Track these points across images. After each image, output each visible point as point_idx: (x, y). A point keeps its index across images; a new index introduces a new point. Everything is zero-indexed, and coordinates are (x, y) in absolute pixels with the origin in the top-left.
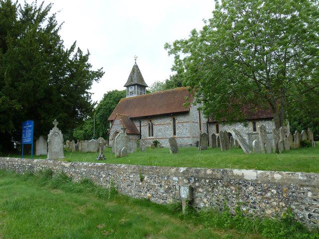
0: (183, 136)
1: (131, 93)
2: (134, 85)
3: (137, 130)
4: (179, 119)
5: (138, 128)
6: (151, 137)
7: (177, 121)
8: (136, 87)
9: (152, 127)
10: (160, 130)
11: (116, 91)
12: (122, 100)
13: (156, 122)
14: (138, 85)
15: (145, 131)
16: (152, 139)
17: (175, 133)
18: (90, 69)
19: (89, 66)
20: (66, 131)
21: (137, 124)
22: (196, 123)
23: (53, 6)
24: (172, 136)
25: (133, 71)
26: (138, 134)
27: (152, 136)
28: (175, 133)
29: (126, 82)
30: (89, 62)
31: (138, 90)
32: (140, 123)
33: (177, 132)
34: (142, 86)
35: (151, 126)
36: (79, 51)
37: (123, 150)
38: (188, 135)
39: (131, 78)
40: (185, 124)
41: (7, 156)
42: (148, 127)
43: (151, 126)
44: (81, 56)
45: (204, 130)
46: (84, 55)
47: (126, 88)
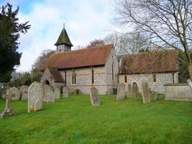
0: (99, 84)
1: (59, 50)
2: (62, 44)
4: (97, 70)
5: (64, 77)
6: (74, 85)
7: (95, 73)
8: (64, 45)
9: (75, 76)
10: (81, 80)
11: (97, 42)
13: (78, 72)
14: (65, 44)
15: (69, 79)
17: (93, 82)
18: (17, 21)
21: (63, 73)
22: (110, 74)
23: (29, 22)
25: (62, 32)
26: (64, 82)
27: (75, 83)
28: (93, 82)
29: (56, 42)
30: (16, 17)
32: (66, 73)
33: (95, 81)
34: (69, 45)
35: (74, 79)
37: (36, 101)
38: (103, 83)
39: (60, 38)
40: (101, 75)
42: (72, 76)
43: (74, 79)
44: (10, 10)
45: (115, 79)
46: (13, 10)
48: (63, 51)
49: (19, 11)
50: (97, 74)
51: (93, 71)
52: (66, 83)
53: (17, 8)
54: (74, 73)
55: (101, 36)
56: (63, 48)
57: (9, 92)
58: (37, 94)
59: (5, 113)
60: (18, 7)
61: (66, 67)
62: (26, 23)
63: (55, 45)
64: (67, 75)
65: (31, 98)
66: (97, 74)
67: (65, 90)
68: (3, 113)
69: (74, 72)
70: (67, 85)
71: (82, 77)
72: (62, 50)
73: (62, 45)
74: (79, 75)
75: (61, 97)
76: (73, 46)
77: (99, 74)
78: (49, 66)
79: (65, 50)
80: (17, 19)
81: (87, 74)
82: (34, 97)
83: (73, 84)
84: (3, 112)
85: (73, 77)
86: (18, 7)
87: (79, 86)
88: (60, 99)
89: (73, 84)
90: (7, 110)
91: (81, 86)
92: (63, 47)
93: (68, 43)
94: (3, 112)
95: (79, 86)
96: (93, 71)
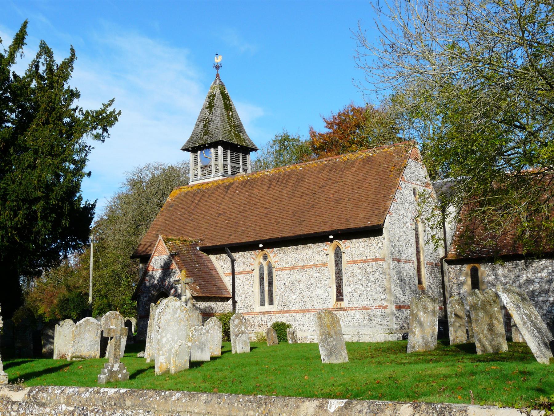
2: (214, 145)
3: (226, 289)
5: (227, 281)
7: (345, 258)
8: (220, 149)
9: (270, 274)
10: (292, 287)
12: (176, 192)
14: (227, 146)
16: (270, 313)
17: (340, 296)
18: (75, 104)
19: (74, 95)
20: (532, 161)
24: (332, 302)
27: (271, 303)
28: (340, 296)
30: (71, 84)
31: (225, 159)
32: (233, 261)
33: (346, 290)
36: (45, 50)
37: (176, 347)
41: (220, 245)
46: (59, 59)
47: (189, 156)
48: (217, 171)
49: (75, 64)
50: (354, 262)
51: (338, 253)
52: (234, 302)
53: (68, 56)
54: (265, 264)
55: (360, 104)
56: (217, 160)
57: (116, 324)
58: (176, 328)
59: (111, 372)
60: (73, 51)
61: (235, 240)
62: (106, 106)
63: (186, 149)
64: (237, 270)
65: (162, 337)
66: (354, 262)
67: (237, 326)
68: (105, 374)
69: (265, 258)
70: (239, 308)
71: (297, 275)
72: (213, 169)
73: (212, 150)
74: (286, 268)
75: (225, 349)
76: (255, 150)
77: (361, 261)
78: (168, 240)
79: (225, 166)
80: (74, 95)
81: (317, 266)
82: (169, 336)
83: (239, 164)
84: (106, 371)
85: (262, 279)
86: (73, 51)
87: (287, 312)
88: (223, 353)
89: (262, 304)
90: (113, 366)
91: (294, 311)
92: (216, 154)
93: (235, 141)
94: (106, 371)
95: (287, 312)
96: (338, 253)
